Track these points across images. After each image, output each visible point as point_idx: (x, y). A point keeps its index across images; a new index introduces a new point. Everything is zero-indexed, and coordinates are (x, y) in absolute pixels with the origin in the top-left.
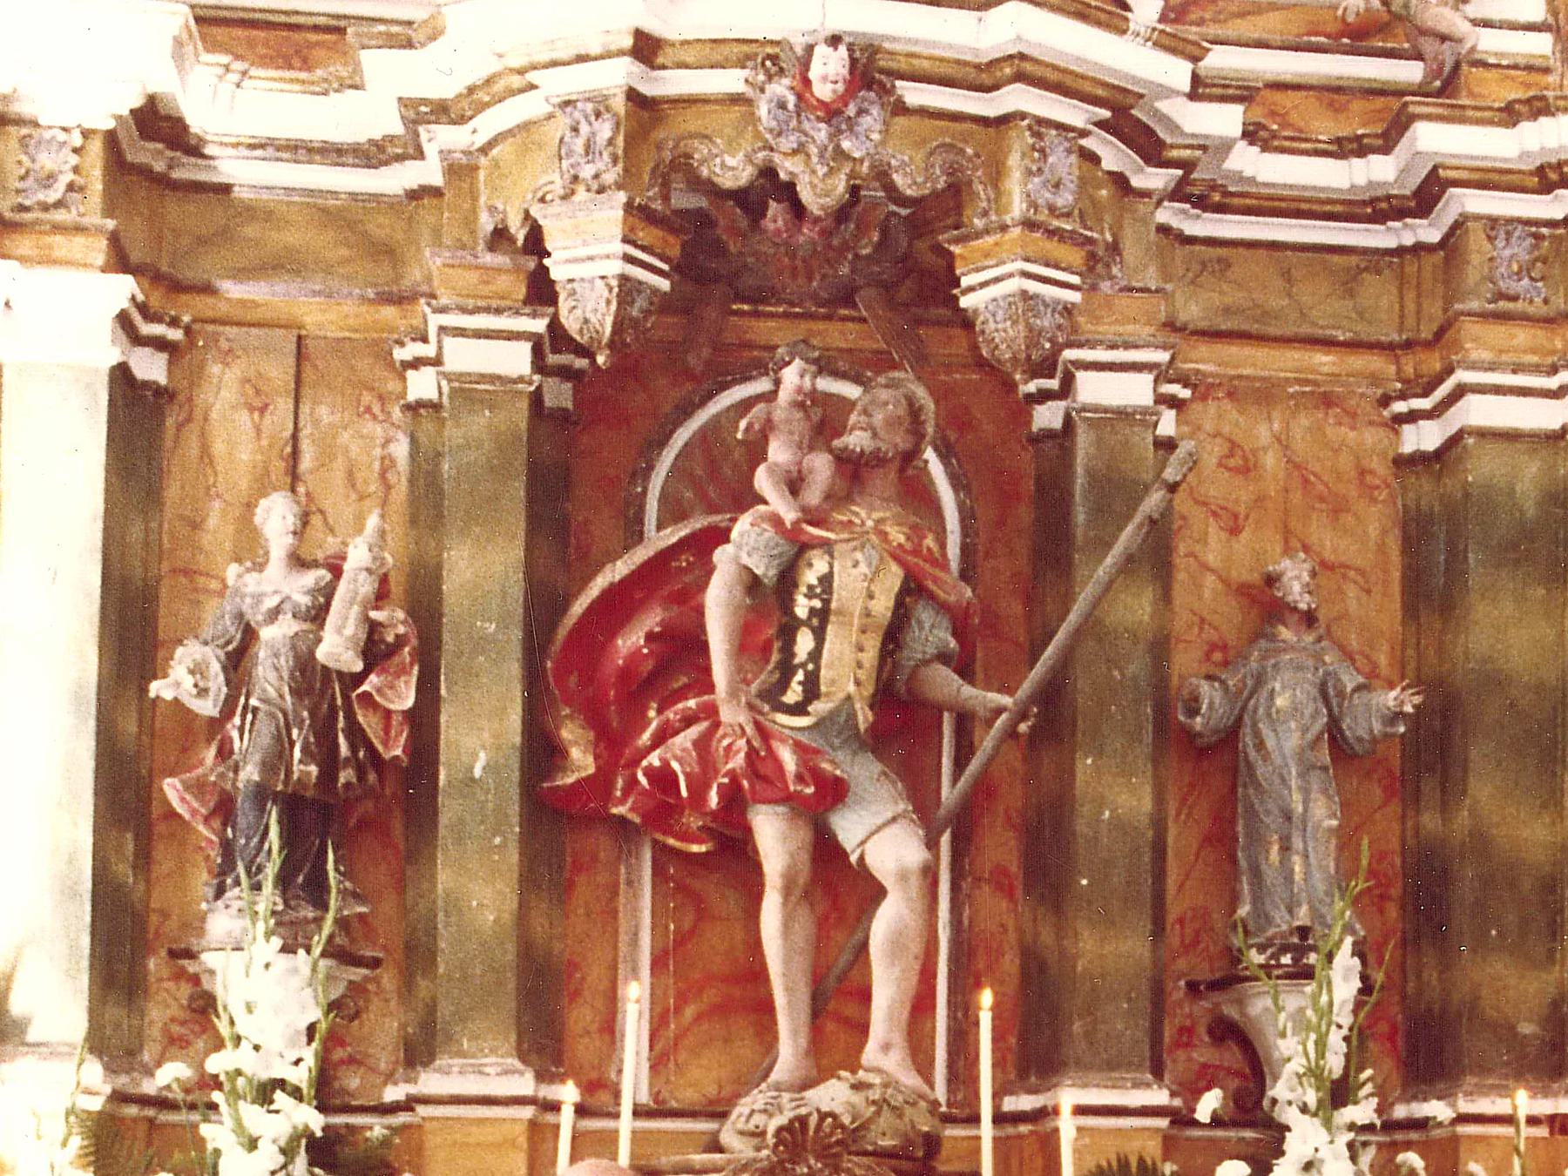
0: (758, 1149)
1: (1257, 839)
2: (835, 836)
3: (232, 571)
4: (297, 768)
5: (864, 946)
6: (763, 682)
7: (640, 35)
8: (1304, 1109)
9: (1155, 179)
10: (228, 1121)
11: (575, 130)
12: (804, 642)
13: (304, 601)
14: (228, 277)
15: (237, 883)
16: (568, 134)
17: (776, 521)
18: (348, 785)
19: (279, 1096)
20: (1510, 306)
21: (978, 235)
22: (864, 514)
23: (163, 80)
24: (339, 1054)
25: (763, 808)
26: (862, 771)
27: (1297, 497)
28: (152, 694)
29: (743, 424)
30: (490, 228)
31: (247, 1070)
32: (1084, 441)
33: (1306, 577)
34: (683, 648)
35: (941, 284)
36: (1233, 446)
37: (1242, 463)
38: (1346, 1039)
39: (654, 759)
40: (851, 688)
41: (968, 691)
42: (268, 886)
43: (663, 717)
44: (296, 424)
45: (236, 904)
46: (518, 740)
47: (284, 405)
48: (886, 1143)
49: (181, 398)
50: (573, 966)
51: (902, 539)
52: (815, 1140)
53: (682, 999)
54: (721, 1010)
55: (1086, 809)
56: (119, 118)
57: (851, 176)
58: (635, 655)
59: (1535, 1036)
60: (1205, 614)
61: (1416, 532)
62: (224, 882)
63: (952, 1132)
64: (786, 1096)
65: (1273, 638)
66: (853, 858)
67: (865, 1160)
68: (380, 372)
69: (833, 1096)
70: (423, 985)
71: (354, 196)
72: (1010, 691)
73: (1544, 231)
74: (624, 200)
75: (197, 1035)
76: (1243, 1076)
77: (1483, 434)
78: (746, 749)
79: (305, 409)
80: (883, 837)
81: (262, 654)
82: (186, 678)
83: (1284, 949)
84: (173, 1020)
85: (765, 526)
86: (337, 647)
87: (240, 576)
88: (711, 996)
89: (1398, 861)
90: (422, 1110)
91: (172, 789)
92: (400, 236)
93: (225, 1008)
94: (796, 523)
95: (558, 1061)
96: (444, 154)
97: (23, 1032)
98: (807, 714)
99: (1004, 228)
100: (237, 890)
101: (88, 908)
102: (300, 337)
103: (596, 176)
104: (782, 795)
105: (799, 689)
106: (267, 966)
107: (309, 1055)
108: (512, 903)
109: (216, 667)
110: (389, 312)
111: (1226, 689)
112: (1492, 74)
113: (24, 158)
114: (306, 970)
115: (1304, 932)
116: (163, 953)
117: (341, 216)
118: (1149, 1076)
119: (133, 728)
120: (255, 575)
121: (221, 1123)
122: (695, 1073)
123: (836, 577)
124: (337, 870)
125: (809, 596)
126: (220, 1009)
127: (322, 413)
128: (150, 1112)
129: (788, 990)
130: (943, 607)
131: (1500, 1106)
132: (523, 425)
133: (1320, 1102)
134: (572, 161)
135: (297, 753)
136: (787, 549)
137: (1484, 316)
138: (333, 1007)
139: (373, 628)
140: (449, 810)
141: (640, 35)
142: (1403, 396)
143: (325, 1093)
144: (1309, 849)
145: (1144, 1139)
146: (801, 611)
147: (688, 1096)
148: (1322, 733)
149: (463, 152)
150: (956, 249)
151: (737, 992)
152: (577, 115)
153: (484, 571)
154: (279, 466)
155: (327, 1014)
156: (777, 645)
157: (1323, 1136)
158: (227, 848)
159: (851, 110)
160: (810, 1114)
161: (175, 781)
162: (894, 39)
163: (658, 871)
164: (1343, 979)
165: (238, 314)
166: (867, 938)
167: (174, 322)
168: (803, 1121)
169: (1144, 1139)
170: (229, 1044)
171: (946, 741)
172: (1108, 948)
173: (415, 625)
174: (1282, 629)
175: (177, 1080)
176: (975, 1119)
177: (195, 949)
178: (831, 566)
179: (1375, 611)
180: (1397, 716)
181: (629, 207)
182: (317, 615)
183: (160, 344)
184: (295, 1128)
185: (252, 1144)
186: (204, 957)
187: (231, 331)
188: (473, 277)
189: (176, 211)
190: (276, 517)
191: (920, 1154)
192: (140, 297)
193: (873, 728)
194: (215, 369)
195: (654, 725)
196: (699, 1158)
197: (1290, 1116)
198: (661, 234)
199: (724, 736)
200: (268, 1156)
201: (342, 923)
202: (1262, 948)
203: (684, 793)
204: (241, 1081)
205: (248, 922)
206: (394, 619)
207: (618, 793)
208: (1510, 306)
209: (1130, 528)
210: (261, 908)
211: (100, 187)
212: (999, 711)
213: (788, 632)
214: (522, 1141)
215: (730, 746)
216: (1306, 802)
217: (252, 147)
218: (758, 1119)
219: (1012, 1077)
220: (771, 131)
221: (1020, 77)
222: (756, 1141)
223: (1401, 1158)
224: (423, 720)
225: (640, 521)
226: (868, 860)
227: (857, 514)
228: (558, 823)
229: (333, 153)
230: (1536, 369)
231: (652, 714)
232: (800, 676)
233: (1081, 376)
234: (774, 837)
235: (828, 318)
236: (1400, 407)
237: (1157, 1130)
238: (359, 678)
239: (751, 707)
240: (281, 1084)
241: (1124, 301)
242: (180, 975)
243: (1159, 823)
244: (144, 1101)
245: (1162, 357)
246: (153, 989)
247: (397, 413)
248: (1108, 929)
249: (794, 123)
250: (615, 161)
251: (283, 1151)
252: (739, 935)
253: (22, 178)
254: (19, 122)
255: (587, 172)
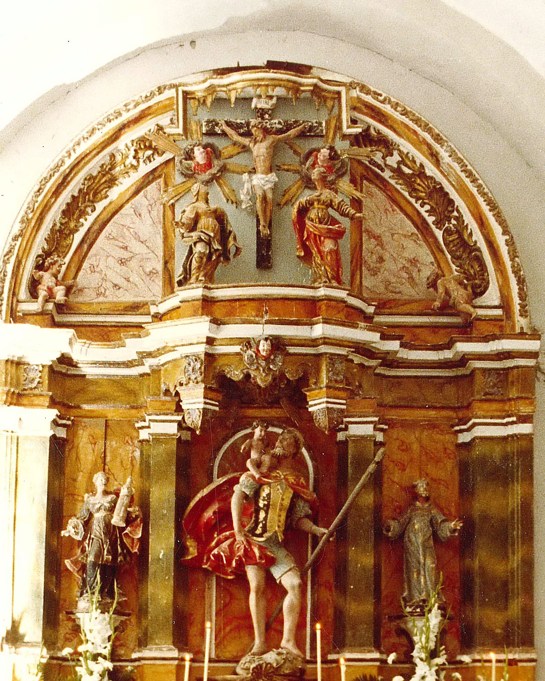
0: (248, 674)
1: (409, 571)
2: (272, 575)
3: (86, 495)
4: (105, 557)
5: (281, 610)
6: (250, 527)
7: (208, 338)
8: (421, 660)
9: (373, 363)
10: (84, 666)
11: (189, 364)
12: (262, 515)
13: (108, 505)
14: (85, 403)
15: (87, 592)
16: (187, 365)
17: (253, 477)
18: (121, 561)
19: (100, 658)
20: (490, 397)
21: (313, 390)
22: (280, 473)
23: (66, 350)
24: (118, 643)
25: (250, 566)
26: (280, 554)
27: (424, 458)
28: (62, 535)
29: (243, 447)
30: (165, 389)
31: (90, 650)
32: (351, 445)
33: (425, 486)
34: (224, 515)
35: (303, 401)
36: (403, 442)
37: (405, 448)
38: (436, 636)
39: (215, 551)
40: (277, 528)
41: (315, 527)
42: (97, 594)
43: (219, 537)
44: (105, 446)
45: (87, 598)
46: (173, 546)
47: (102, 442)
48: (287, 672)
49: (70, 442)
50: (191, 615)
51: (293, 481)
52: (265, 671)
53: (226, 625)
54: (238, 628)
55: (353, 564)
56: (53, 361)
57: (273, 376)
58: (210, 519)
59: (501, 633)
60: (394, 497)
61: (464, 468)
62: (83, 591)
63: (309, 666)
64: (256, 657)
65: (415, 505)
66: (278, 582)
67: (280, 678)
68: (131, 431)
69: (271, 657)
70: (144, 623)
71: (123, 376)
72: (327, 527)
73: (502, 372)
74: (204, 386)
75: (74, 638)
76: (407, 647)
77: (482, 439)
78: (243, 549)
79: (108, 443)
80: (287, 576)
81: (95, 522)
82: (72, 529)
83: (417, 607)
84: (67, 633)
85: (249, 478)
86: (117, 520)
87: (88, 497)
88: (235, 624)
89: (458, 575)
90: (143, 662)
91: (68, 563)
92: (137, 388)
93: (84, 631)
94: (259, 478)
95: (186, 645)
96: (150, 366)
97: (23, 639)
98: (262, 537)
99: (321, 388)
100: (87, 595)
101: (43, 600)
102: (106, 421)
103: (196, 378)
104: (254, 562)
105: (260, 529)
106: (96, 618)
107: (109, 645)
108: (171, 597)
109: (81, 526)
110: (134, 411)
111: (399, 522)
112: (484, 323)
113: (25, 374)
114: (108, 619)
115: (424, 601)
116: (64, 613)
117: (119, 383)
118: (373, 649)
119: (55, 543)
120: (93, 497)
121: (81, 666)
122: (229, 648)
123: (272, 494)
124: (117, 587)
125: (263, 500)
126: (82, 632)
127: (113, 443)
128: (60, 662)
129: (258, 622)
130: (306, 501)
131: (485, 657)
132: (175, 449)
133: (427, 657)
134: (189, 373)
135: (105, 552)
136: (256, 486)
137: (481, 401)
138: (116, 629)
139: (129, 513)
140: (152, 568)
141: (208, 338)
142: (458, 425)
143: (114, 657)
144: (425, 575)
145: (372, 669)
146: (261, 504)
147: (228, 655)
148: (430, 536)
149: (156, 366)
150: (308, 394)
151: (242, 622)
152: (190, 360)
153: (163, 494)
154: (100, 461)
155: (115, 631)
156: (254, 515)
157: (427, 668)
158: (84, 580)
159: (272, 357)
160: (263, 663)
161: (69, 561)
162: (286, 336)
163: (218, 584)
164: (434, 619)
165: (88, 414)
166: (282, 605)
167: (69, 419)
168: (260, 666)
169: (372, 669)
170: (84, 643)
171: (310, 540)
172: (360, 608)
173: (141, 513)
174: (418, 503)
175: (69, 653)
176: (316, 662)
177: (74, 612)
178: (270, 490)
179: (450, 494)
180: (455, 530)
181: (205, 388)
182: (111, 509)
183: (64, 426)
184: (104, 668)
185: (91, 673)
186: (77, 614)
187: (86, 420)
188: (159, 404)
189: (69, 383)
190: (99, 480)
191: (298, 674)
192: (59, 414)
193: (283, 541)
194: (81, 432)
195: (216, 539)
196: (229, 677)
197: (417, 661)
198: (215, 394)
199: (238, 544)
200: (96, 677)
201: (118, 603)
202: (410, 607)
203: (225, 562)
204: (88, 654)
205: (90, 604)
206: (135, 510)
207: (205, 561)
208: (490, 397)
209: (364, 476)
210: (95, 600)
211: (47, 382)
212: (324, 534)
213: (257, 511)
214: (174, 671)
215: (238, 548)
216: (425, 560)
217: (91, 364)
218: (247, 665)
219: (331, 648)
220: (248, 364)
221: (325, 343)
222: (246, 671)
223: (453, 674)
224: (144, 541)
225: (212, 474)
226: (282, 582)
227: (278, 473)
228: (186, 573)
229: (117, 364)
230: (499, 417)
231: (215, 535)
232: (261, 525)
233: (350, 426)
234: (252, 574)
235: (271, 408)
236: (457, 428)
237: (376, 666)
238: (124, 529)
239: (245, 535)
240: (99, 655)
241: (364, 402)
242: (69, 619)
243: (377, 567)
244: (58, 659)
245: (376, 419)
246: (61, 623)
247: (136, 442)
248: (360, 601)
249: (255, 361)
250: (201, 375)
251: (100, 675)
252: (244, 605)
253: (25, 381)
254: (24, 364)
255: (193, 377)
